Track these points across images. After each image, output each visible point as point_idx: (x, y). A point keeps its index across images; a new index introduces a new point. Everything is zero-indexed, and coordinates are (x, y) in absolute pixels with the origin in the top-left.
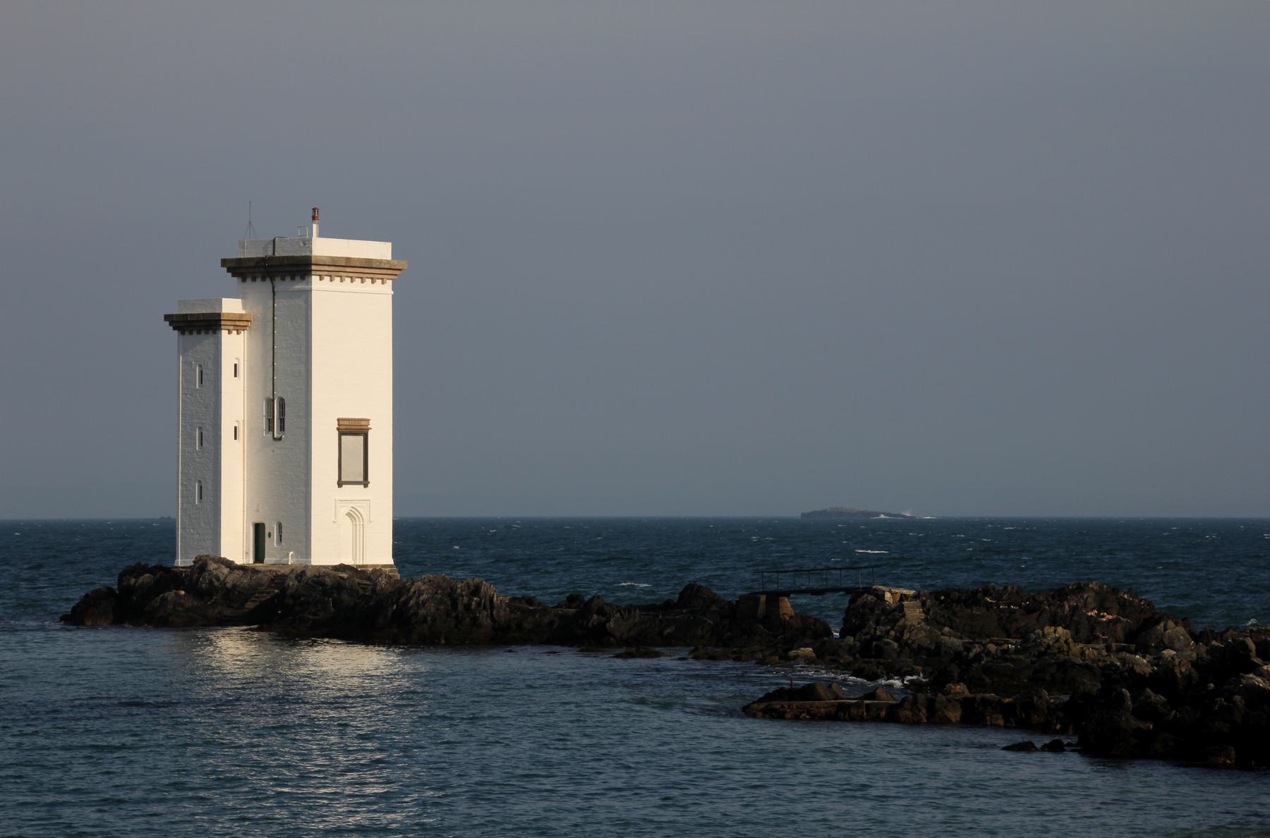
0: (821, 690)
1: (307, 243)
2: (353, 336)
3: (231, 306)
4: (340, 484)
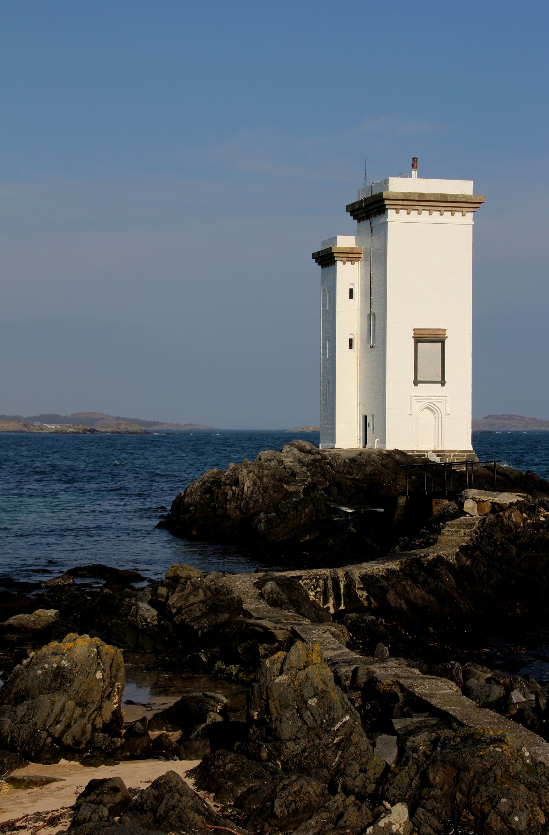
4: (416, 382)
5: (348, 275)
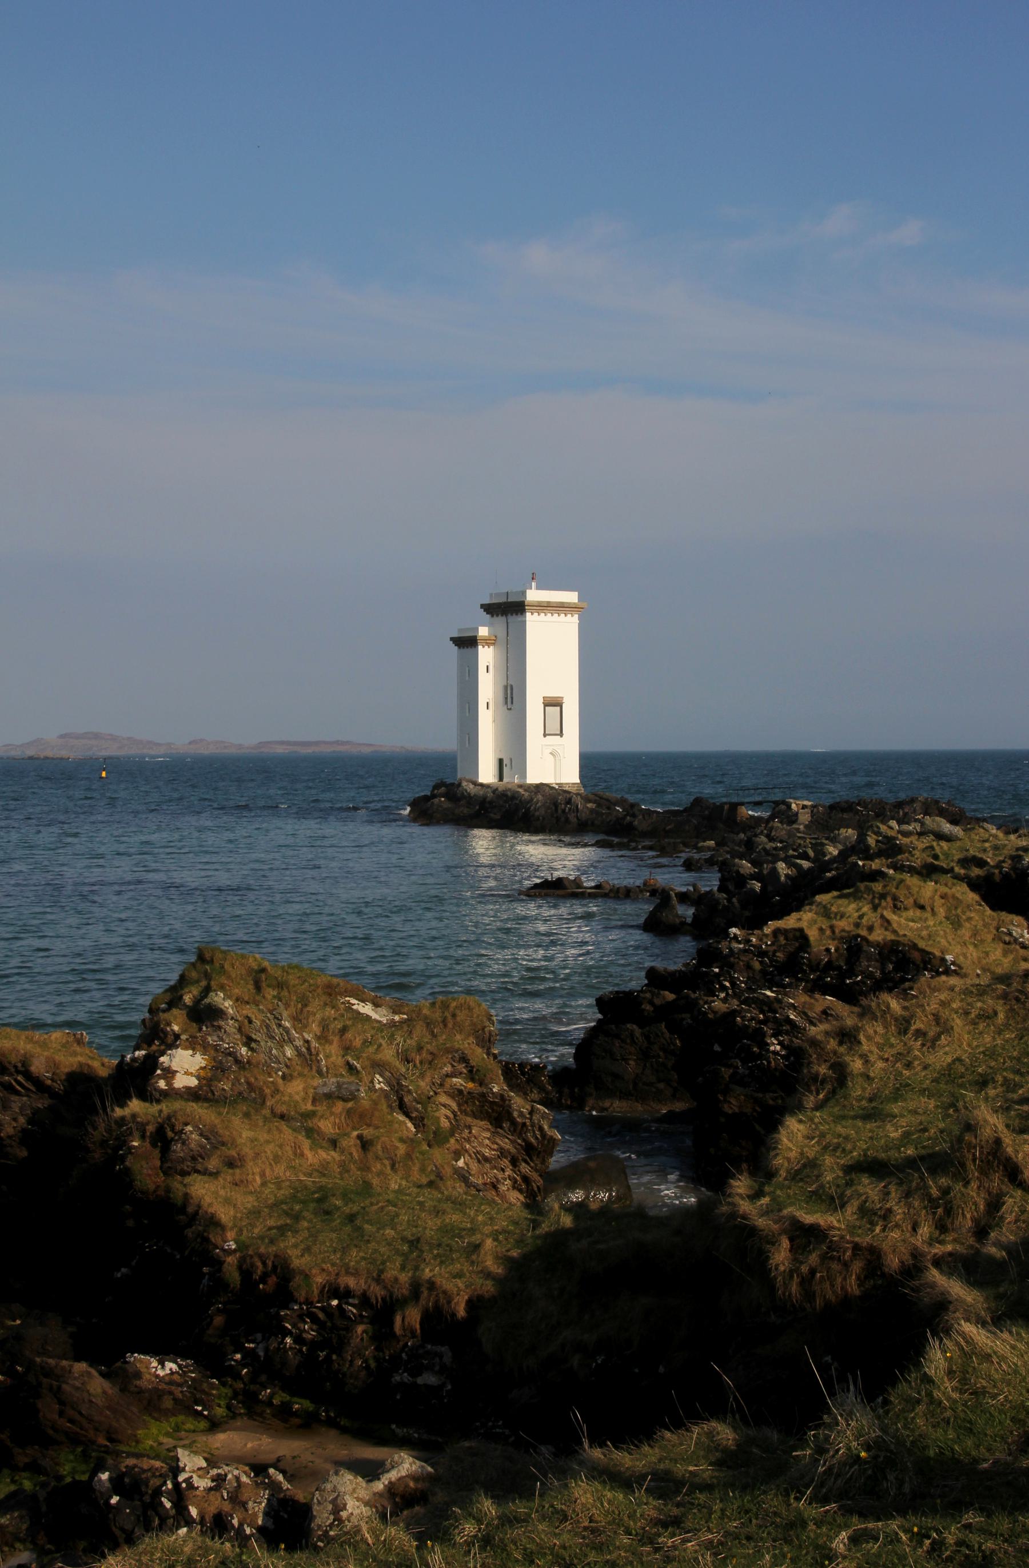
0: (604, 885)
1: (524, 593)
2: (554, 647)
3: (483, 632)
4: (545, 735)
5: (486, 655)
